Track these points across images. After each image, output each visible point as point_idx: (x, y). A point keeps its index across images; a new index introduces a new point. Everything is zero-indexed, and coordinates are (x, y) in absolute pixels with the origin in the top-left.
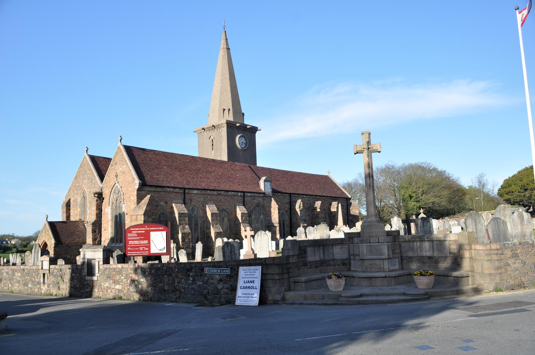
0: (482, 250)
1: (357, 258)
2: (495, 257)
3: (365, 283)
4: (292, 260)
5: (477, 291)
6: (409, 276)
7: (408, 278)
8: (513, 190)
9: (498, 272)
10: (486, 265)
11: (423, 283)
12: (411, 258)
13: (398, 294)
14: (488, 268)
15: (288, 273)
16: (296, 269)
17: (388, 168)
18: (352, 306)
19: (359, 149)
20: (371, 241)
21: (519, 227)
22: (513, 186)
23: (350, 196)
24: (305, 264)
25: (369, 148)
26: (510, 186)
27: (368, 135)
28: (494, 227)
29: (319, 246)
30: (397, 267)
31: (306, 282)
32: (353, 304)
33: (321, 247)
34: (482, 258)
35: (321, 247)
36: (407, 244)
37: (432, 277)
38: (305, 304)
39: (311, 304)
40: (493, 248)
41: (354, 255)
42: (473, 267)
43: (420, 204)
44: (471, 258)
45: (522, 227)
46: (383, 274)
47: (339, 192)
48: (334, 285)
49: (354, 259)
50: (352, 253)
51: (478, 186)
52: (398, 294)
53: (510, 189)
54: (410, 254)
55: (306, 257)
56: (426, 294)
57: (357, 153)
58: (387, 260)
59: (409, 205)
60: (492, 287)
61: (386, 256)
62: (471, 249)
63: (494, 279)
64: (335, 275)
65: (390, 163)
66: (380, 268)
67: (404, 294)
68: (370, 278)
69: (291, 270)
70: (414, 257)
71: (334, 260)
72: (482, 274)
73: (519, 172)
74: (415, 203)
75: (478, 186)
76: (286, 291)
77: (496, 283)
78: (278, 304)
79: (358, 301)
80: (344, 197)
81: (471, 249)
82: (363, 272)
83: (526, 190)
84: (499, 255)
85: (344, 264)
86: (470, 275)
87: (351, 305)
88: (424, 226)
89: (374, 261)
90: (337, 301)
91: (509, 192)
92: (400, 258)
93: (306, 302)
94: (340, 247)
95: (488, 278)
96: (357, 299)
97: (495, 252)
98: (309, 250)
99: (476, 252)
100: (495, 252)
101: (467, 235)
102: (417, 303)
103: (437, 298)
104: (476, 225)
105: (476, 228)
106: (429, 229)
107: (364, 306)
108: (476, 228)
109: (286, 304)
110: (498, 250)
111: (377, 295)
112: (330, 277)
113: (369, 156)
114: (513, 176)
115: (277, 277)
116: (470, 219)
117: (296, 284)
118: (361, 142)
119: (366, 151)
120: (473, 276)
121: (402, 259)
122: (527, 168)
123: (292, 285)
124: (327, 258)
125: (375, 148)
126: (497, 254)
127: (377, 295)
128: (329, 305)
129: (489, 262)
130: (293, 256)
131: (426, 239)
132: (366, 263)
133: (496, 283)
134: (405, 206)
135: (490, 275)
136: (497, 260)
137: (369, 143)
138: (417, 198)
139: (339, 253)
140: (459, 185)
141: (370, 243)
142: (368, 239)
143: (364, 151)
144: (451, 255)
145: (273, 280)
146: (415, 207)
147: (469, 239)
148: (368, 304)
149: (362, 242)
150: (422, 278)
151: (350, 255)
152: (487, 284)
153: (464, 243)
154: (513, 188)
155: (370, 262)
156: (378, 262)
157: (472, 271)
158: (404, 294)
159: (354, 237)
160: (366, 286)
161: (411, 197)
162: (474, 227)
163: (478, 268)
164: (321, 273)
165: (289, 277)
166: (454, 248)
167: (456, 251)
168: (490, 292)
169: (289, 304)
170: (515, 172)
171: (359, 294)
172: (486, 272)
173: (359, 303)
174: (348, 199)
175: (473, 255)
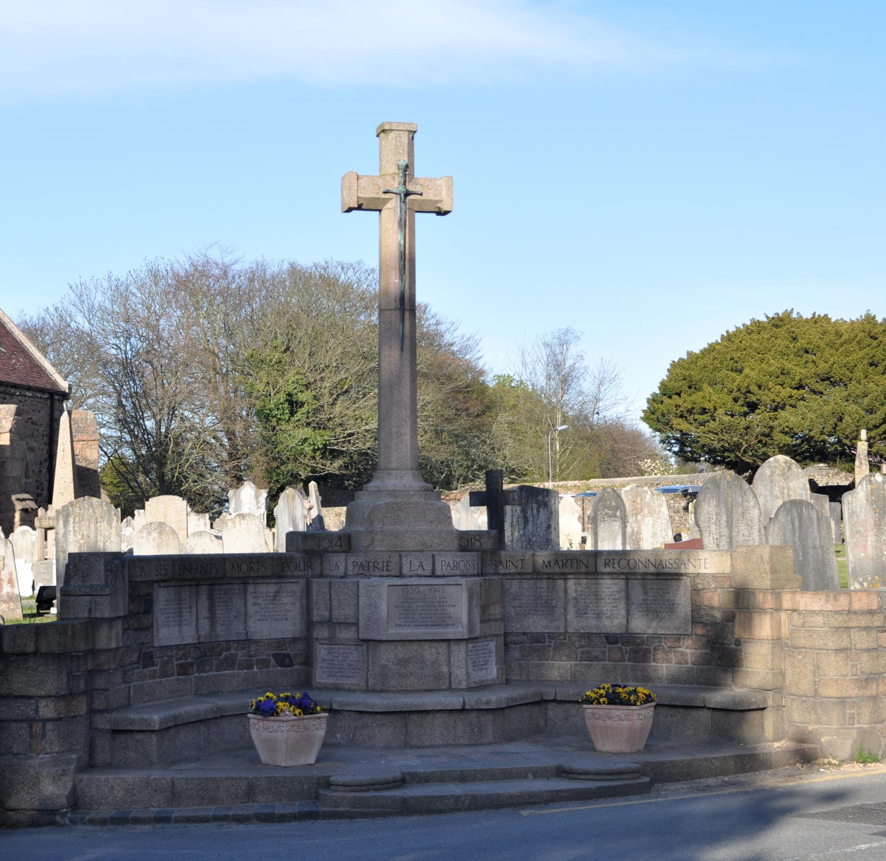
0: (820, 612)
1: (346, 634)
2: (862, 640)
3: (384, 733)
4: (108, 639)
5: (806, 756)
6: (536, 709)
7: (537, 714)
8: (708, 405)
9: (868, 693)
10: (833, 666)
11: (619, 731)
12: (538, 638)
13: (538, 774)
14: (837, 676)
15: (90, 692)
16: (119, 675)
17: (204, 274)
18: (380, 821)
19: (369, 192)
20: (406, 570)
21: (871, 539)
22: (707, 389)
23: (64, 385)
24: (147, 659)
25: (407, 194)
26: (693, 387)
27: (405, 138)
28: (789, 535)
29: (196, 584)
30: (492, 672)
31: (164, 730)
32: (384, 815)
33: (204, 589)
34: (818, 643)
35: (204, 589)
36: (526, 584)
37: (648, 711)
38: (179, 820)
39: (205, 820)
40: (857, 606)
41: (330, 623)
42: (783, 675)
43: (327, 435)
44: (777, 641)
45: (878, 540)
46: (454, 701)
47: (17, 361)
48: (286, 741)
49: (332, 641)
50: (320, 612)
51: (542, 381)
52: (538, 774)
53: (697, 397)
54: (538, 624)
55: (149, 628)
56: (639, 772)
57: (360, 208)
58: (463, 646)
59: (281, 437)
60: (846, 748)
61: (460, 631)
62: (779, 609)
63: (852, 717)
64: (286, 699)
65: (215, 255)
66: (438, 677)
67: (562, 773)
68: (404, 714)
69: (100, 682)
70: (551, 636)
71: (247, 642)
72: (814, 700)
73: (729, 338)
74: (307, 432)
75: (542, 381)
76: (80, 770)
77: (862, 732)
78: (53, 823)
79: (405, 800)
80: (40, 383)
81: (779, 609)
82: (368, 690)
83: (753, 407)
84: (874, 633)
85: (283, 660)
86: (770, 703)
87: (373, 816)
88: (526, 521)
89: (415, 647)
90: (312, 801)
91: (690, 411)
92: (501, 640)
93: (176, 813)
94: (272, 589)
95: (835, 715)
96: (398, 793)
97: (864, 621)
98: (162, 597)
99: (797, 619)
100: (864, 621)
101: (766, 557)
102: (621, 803)
103: (679, 785)
104: (730, 525)
105: (731, 537)
106: (541, 532)
107: (425, 818)
108: (731, 537)
109: (92, 822)
110: (871, 612)
111: (462, 777)
112: (267, 711)
113: (406, 225)
114: (705, 352)
115: (47, 710)
116: (714, 502)
117: (121, 738)
118: (374, 165)
119: (394, 203)
120: (779, 707)
121: (507, 642)
122: (757, 324)
123: (103, 742)
124: (222, 634)
125: (429, 195)
126: (867, 629)
127: (462, 777)
128: (283, 819)
129: (842, 656)
130: (111, 621)
131: (601, 568)
132: (386, 656)
133: (862, 732)
134: (270, 442)
135: (842, 701)
136: (868, 650)
137: (407, 170)
138: (317, 411)
139: (271, 618)
140: (469, 368)
141: (400, 575)
142: (395, 559)
143: (386, 201)
144: (699, 631)
145: (30, 721)
146: (308, 449)
147: (774, 571)
148: (440, 811)
149: (367, 570)
150: (618, 711)
151: (309, 624)
152: (833, 734)
153: (756, 584)
154: (708, 396)
155: (401, 652)
156: (429, 652)
157: (779, 690)
158: (562, 773)
159: (326, 551)
160: (388, 747)
161: (294, 405)
162: (725, 531)
163: (799, 677)
164: (199, 693)
165: (92, 712)
166: (716, 599)
167: (718, 615)
168: (842, 762)
169: (103, 822)
170: (715, 337)
171: (398, 774)
172: (831, 691)
173: (407, 808)
174: (55, 399)
175: (785, 631)
